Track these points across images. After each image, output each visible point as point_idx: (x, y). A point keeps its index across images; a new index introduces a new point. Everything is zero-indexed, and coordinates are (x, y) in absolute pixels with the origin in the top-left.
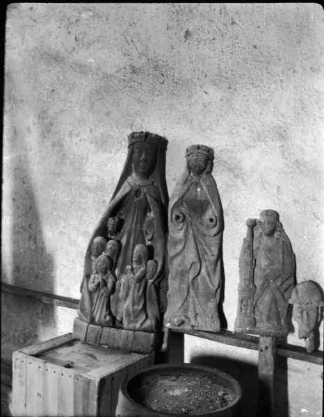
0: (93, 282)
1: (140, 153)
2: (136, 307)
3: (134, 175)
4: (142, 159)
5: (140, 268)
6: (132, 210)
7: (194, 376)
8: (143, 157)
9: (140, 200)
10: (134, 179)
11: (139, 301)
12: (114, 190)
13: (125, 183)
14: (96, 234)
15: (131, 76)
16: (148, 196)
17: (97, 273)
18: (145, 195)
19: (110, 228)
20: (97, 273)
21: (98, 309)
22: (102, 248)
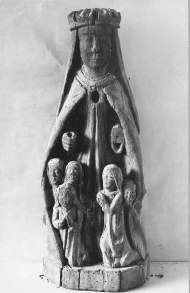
0: (58, 218)
1: (90, 41)
2: (118, 242)
3: (85, 68)
4: (93, 50)
5: (115, 195)
6: (89, 93)
7: (97, 60)
8: (94, 46)
9: (99, 105)
10: (85, 79)
11: (121, 235)
12: (60, 101)
13: (75, 85)
14: (51, 156)
15: (58, 188)
16: (109, 98)
17: (60, 205)
18: (105, 98)
19: (66, 147)
20: (60, 205)
21: (69, 248)
22: (60, 177)
